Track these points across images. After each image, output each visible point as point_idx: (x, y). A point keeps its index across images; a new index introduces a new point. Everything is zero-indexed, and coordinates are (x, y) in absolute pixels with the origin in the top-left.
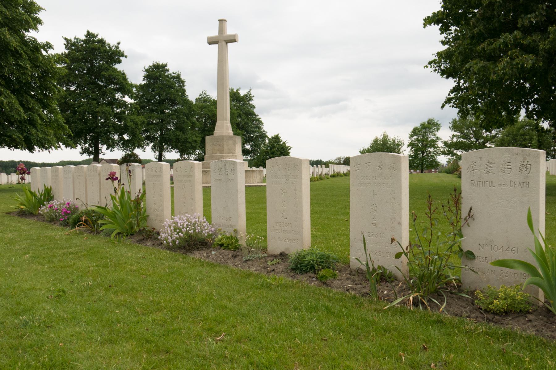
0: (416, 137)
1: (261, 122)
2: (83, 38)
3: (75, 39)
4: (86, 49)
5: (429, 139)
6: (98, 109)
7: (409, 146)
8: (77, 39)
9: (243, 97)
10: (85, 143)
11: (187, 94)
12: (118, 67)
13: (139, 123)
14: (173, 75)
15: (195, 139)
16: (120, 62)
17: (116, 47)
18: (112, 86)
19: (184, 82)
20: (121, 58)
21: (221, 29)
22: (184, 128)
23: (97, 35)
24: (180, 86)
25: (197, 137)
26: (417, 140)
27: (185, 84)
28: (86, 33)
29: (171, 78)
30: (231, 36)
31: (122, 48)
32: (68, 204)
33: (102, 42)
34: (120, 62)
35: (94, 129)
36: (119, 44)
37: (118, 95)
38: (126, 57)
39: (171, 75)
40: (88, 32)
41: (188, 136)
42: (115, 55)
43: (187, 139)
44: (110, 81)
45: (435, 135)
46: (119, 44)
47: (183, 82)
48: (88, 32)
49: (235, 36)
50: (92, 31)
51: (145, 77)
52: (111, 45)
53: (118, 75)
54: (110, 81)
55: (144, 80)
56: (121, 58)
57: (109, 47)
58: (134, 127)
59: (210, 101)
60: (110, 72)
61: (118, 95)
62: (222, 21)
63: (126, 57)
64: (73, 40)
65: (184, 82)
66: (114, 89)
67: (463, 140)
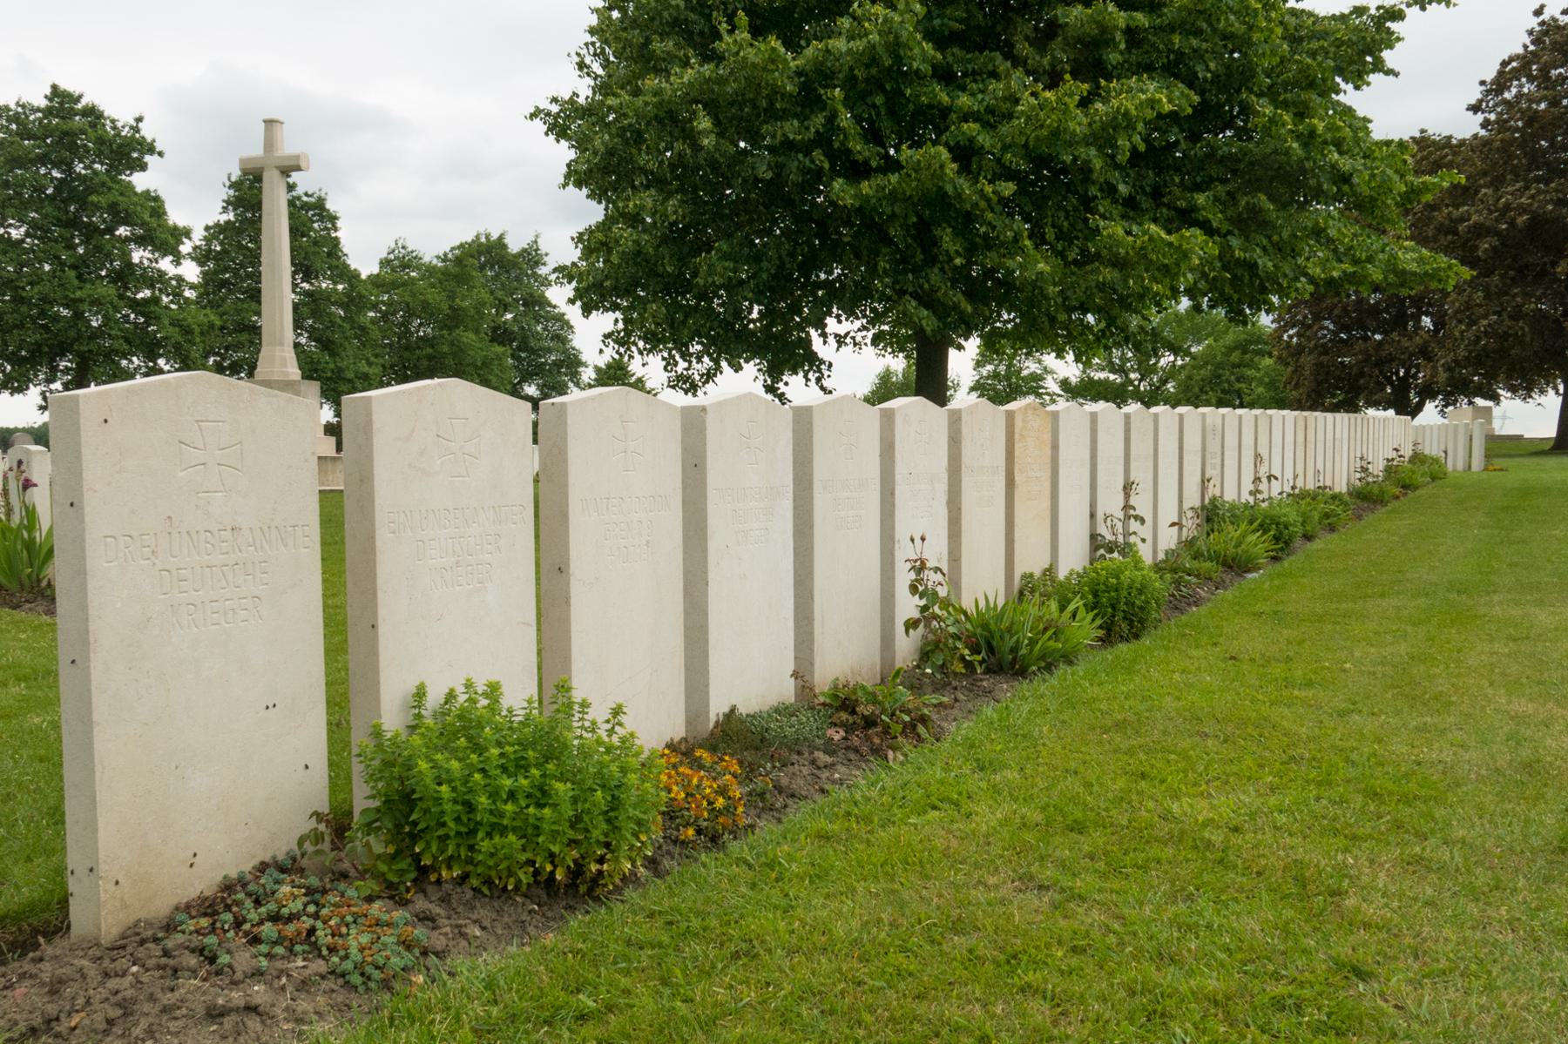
0: (990, 368)
1: (567, 323)
2: (43, 103)
3: (18, 104)
4: (47, 131)
5: (1025, 373)
6: (78, 294)
7: (972, 389)
8: (23, 106)
9: (515, 256)
10: (49, 381)
11: (345, 250)
12: (140, 181)
13: (197, 330)
14: (305, 199)
15: (366, 369)
16: (143, 167)
17: (132, 127)
18: (122, 231)
19: (336, 218)
20: (147, 158)
21: (269, 143)
22: (333, 342)
23: (80, 97)
24: (326, 229)
25: (370, 364)
26: (995, 375)
27: (339, 224)
28: (48, 91)
29: (302, 208)
30: (290, 157)
31: (147, 132)
32: (632, 735)
33: (93, 113)
34: (143, 167)
35: (72, 345)
36: (139, 120)
37: (138, 255)
38: (161, 154)
39: (299, 198)
40: (54, 87)
41: (343, 365)
42: (129, 150)
43: (340, 370)
44: (121, 215)
45: (1040, 362)
46: (139, 120)
47: (333, 219)
48: (54, 87)
49: (298, 157)
50: (66, 85)
51: (228, 202)
52: (119, 125)
53: (135, 204)
54: (121, 215)
55: (225, 210)
56: (147, 158)
57: (114, 128)
58: (181, 339)
59: (418, 268)
60: (114, 197)
61: (138, 255)
62: (269, 123)
63: (161, 154)
64: (13, 106)
65: (336, 218)
66: (127, 240)
67: (1112, 377)
